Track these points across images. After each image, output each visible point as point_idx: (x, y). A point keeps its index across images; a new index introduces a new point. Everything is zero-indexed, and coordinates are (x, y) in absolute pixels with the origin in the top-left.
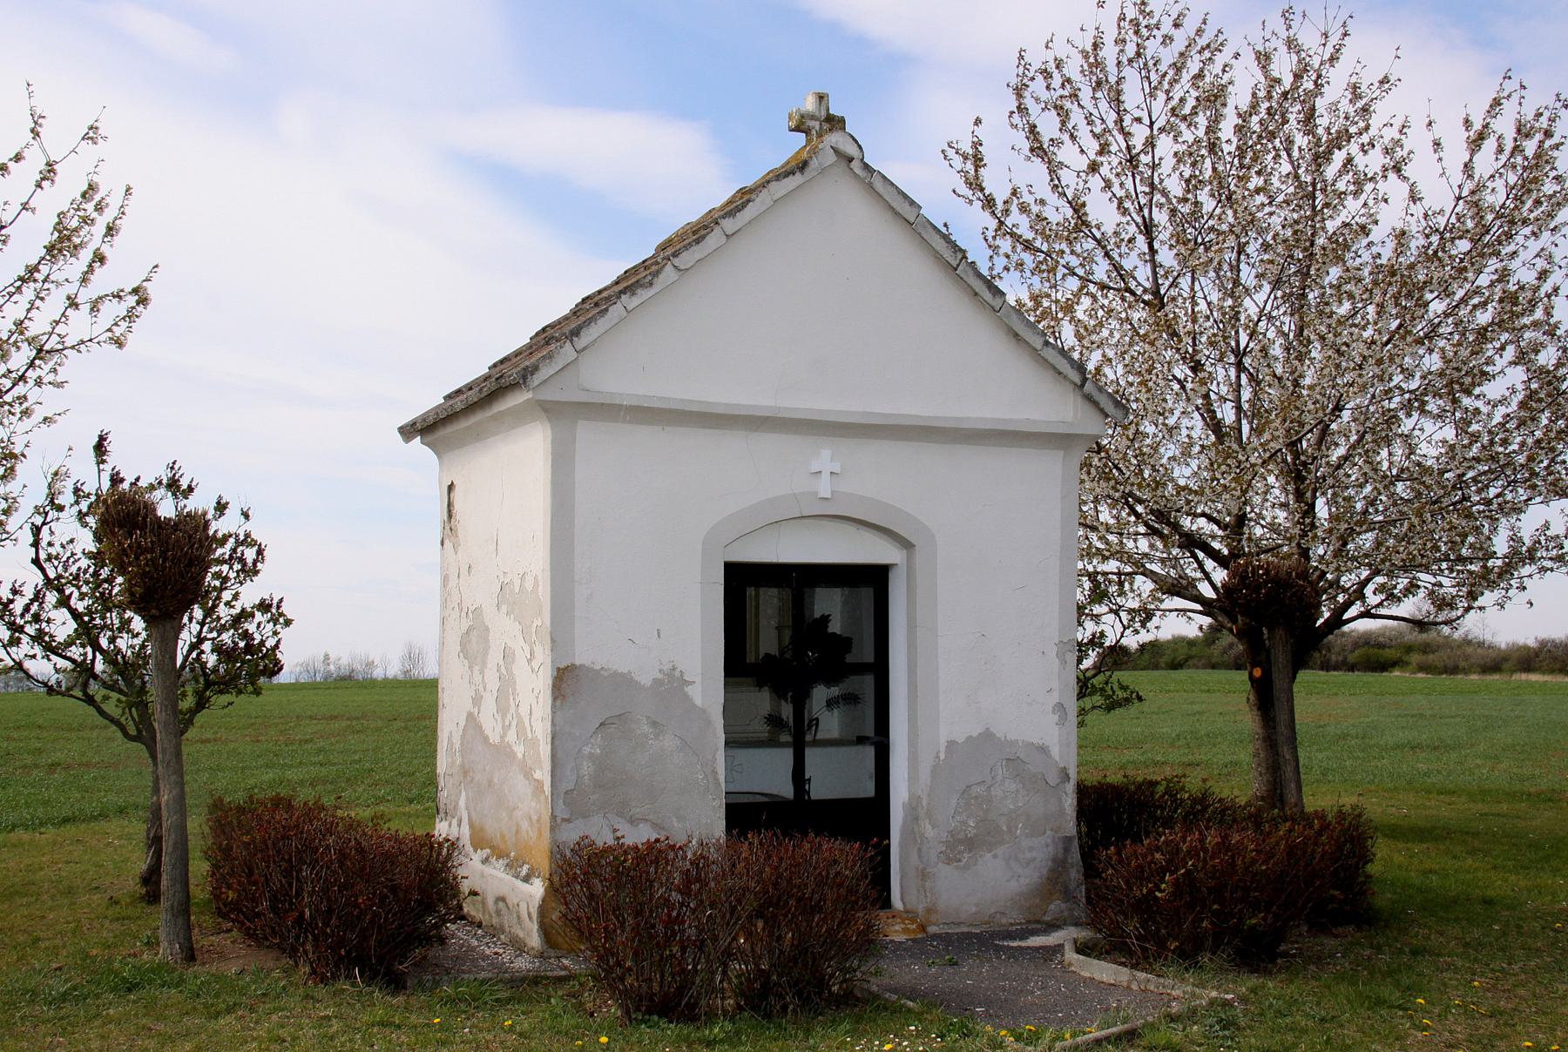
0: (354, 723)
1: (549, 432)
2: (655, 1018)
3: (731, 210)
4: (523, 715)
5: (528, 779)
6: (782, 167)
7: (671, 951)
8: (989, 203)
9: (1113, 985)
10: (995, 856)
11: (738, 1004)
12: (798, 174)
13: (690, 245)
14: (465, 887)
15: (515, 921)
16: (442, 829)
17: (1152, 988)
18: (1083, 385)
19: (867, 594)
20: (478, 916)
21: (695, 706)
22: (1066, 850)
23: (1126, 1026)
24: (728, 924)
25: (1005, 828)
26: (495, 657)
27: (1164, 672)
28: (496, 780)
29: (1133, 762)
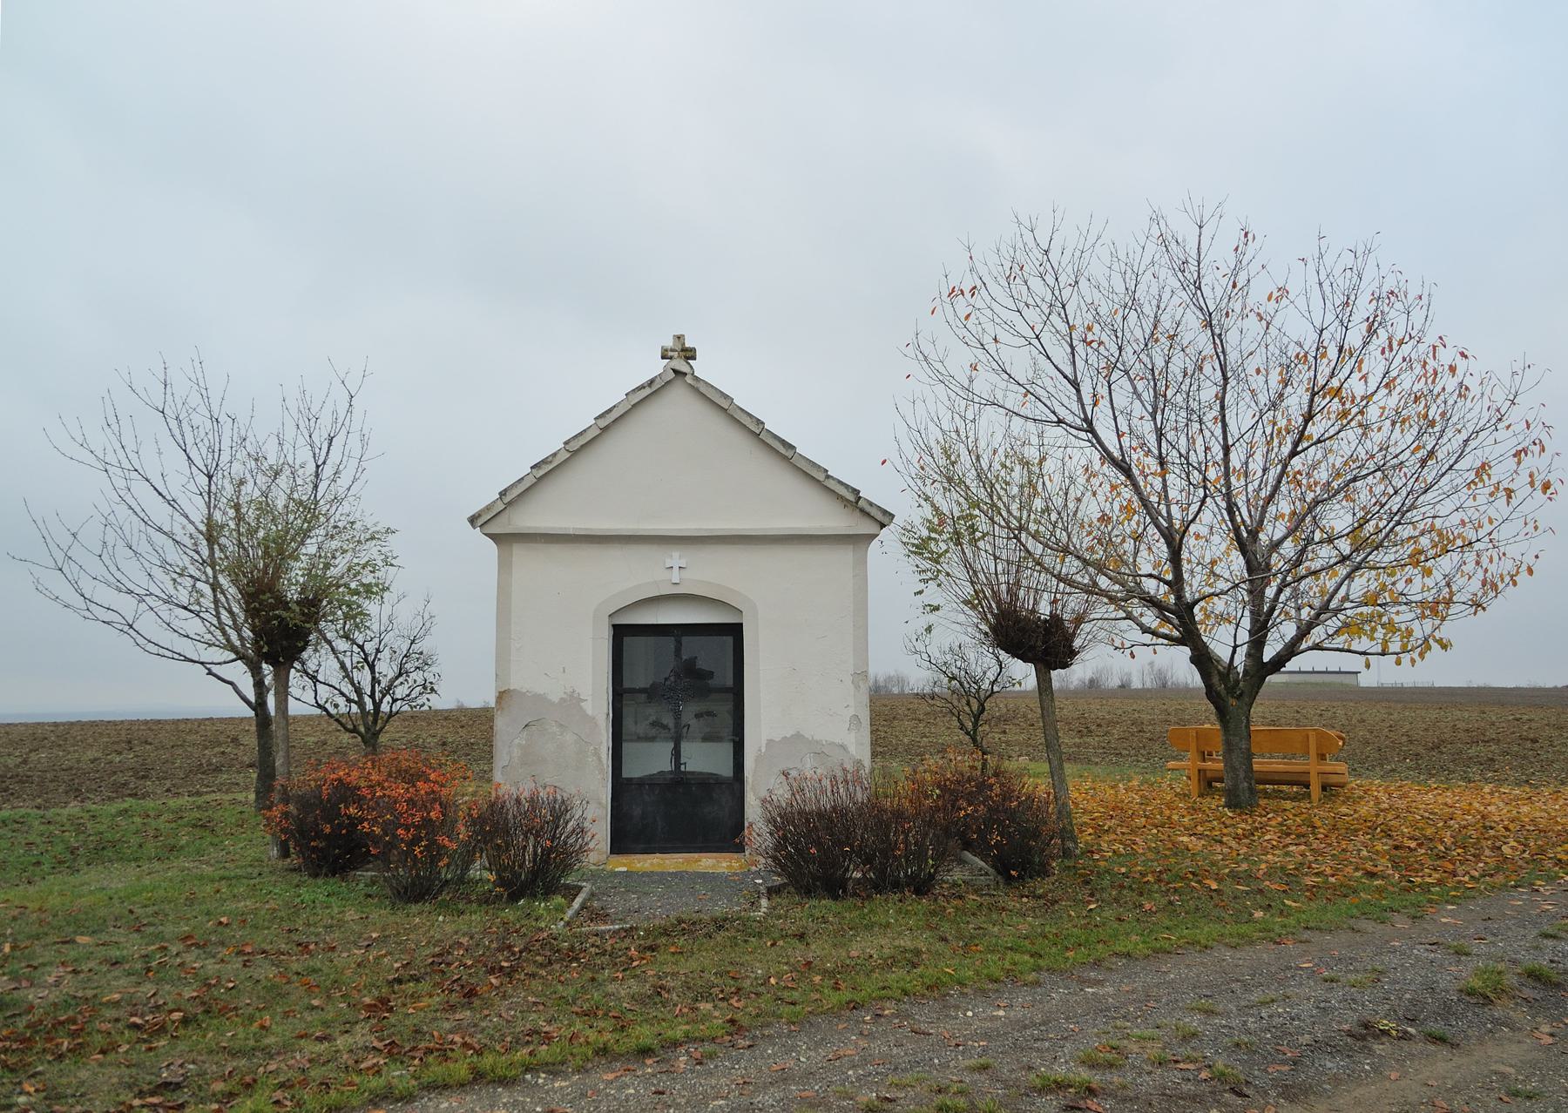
18: (857, 503)
19: (729, 640)
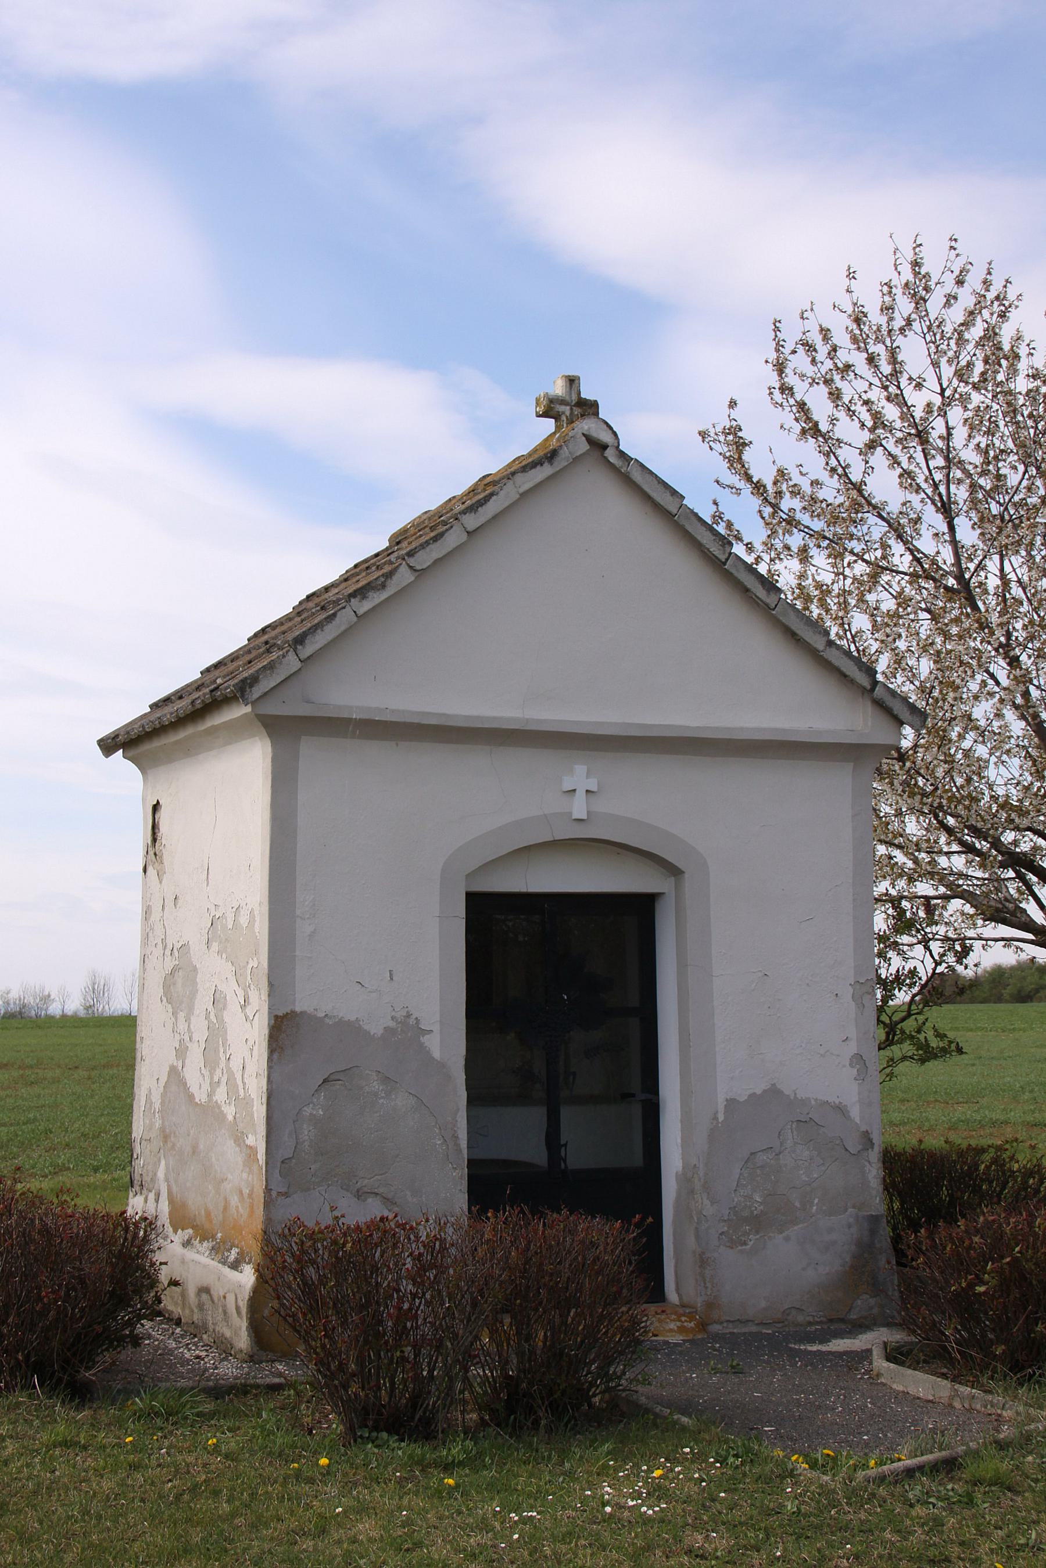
0: (28, 1072)
1: (269, 749)
2: (385, 1435)
3: (473, 505)
4: (234, 1069)
5: (239, 1145)
6: (530, 454)
7: (402, 1352)
8: (759, 488)
9: (930, 1401)
10: (787, 1239)
11: (482, 1419)
12: (546, 464)
13: (427, 543)
14: (164, 1277)
15: (220, 1317)
16: (136, 1205)
17: (978, 1407)
18: (873, 690)
20: (177, 1310)
21: (433, 1058)
22: (873, 1232)
23: (944, 1453)
24: (469, 1320)
25: (797, 1204)
26: (203, 1002)
27: (1010, 1006)
28: (201, 1147)
29: (967, 1121)
